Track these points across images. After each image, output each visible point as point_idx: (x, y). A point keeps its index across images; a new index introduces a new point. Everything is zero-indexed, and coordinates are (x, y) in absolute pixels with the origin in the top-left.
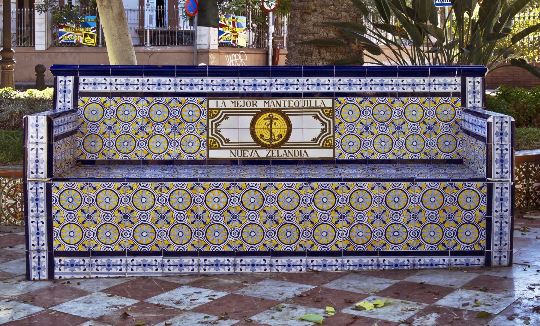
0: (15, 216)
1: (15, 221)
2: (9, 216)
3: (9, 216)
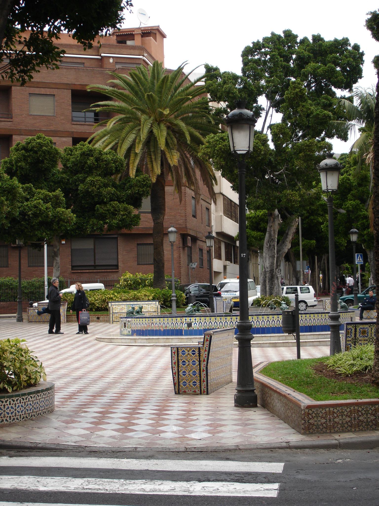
0: (358, 411)
1: (334, 410)
2: (347, 411)
3: (347, 411)
